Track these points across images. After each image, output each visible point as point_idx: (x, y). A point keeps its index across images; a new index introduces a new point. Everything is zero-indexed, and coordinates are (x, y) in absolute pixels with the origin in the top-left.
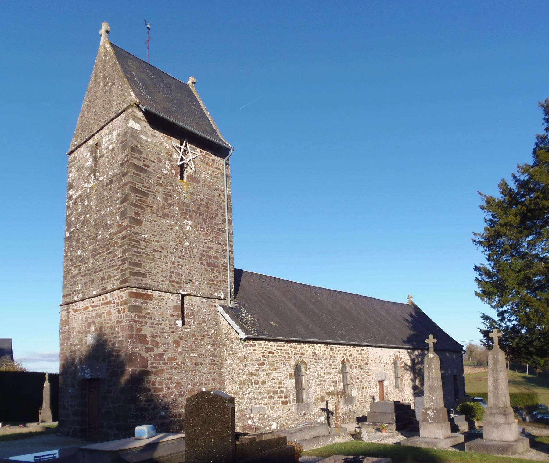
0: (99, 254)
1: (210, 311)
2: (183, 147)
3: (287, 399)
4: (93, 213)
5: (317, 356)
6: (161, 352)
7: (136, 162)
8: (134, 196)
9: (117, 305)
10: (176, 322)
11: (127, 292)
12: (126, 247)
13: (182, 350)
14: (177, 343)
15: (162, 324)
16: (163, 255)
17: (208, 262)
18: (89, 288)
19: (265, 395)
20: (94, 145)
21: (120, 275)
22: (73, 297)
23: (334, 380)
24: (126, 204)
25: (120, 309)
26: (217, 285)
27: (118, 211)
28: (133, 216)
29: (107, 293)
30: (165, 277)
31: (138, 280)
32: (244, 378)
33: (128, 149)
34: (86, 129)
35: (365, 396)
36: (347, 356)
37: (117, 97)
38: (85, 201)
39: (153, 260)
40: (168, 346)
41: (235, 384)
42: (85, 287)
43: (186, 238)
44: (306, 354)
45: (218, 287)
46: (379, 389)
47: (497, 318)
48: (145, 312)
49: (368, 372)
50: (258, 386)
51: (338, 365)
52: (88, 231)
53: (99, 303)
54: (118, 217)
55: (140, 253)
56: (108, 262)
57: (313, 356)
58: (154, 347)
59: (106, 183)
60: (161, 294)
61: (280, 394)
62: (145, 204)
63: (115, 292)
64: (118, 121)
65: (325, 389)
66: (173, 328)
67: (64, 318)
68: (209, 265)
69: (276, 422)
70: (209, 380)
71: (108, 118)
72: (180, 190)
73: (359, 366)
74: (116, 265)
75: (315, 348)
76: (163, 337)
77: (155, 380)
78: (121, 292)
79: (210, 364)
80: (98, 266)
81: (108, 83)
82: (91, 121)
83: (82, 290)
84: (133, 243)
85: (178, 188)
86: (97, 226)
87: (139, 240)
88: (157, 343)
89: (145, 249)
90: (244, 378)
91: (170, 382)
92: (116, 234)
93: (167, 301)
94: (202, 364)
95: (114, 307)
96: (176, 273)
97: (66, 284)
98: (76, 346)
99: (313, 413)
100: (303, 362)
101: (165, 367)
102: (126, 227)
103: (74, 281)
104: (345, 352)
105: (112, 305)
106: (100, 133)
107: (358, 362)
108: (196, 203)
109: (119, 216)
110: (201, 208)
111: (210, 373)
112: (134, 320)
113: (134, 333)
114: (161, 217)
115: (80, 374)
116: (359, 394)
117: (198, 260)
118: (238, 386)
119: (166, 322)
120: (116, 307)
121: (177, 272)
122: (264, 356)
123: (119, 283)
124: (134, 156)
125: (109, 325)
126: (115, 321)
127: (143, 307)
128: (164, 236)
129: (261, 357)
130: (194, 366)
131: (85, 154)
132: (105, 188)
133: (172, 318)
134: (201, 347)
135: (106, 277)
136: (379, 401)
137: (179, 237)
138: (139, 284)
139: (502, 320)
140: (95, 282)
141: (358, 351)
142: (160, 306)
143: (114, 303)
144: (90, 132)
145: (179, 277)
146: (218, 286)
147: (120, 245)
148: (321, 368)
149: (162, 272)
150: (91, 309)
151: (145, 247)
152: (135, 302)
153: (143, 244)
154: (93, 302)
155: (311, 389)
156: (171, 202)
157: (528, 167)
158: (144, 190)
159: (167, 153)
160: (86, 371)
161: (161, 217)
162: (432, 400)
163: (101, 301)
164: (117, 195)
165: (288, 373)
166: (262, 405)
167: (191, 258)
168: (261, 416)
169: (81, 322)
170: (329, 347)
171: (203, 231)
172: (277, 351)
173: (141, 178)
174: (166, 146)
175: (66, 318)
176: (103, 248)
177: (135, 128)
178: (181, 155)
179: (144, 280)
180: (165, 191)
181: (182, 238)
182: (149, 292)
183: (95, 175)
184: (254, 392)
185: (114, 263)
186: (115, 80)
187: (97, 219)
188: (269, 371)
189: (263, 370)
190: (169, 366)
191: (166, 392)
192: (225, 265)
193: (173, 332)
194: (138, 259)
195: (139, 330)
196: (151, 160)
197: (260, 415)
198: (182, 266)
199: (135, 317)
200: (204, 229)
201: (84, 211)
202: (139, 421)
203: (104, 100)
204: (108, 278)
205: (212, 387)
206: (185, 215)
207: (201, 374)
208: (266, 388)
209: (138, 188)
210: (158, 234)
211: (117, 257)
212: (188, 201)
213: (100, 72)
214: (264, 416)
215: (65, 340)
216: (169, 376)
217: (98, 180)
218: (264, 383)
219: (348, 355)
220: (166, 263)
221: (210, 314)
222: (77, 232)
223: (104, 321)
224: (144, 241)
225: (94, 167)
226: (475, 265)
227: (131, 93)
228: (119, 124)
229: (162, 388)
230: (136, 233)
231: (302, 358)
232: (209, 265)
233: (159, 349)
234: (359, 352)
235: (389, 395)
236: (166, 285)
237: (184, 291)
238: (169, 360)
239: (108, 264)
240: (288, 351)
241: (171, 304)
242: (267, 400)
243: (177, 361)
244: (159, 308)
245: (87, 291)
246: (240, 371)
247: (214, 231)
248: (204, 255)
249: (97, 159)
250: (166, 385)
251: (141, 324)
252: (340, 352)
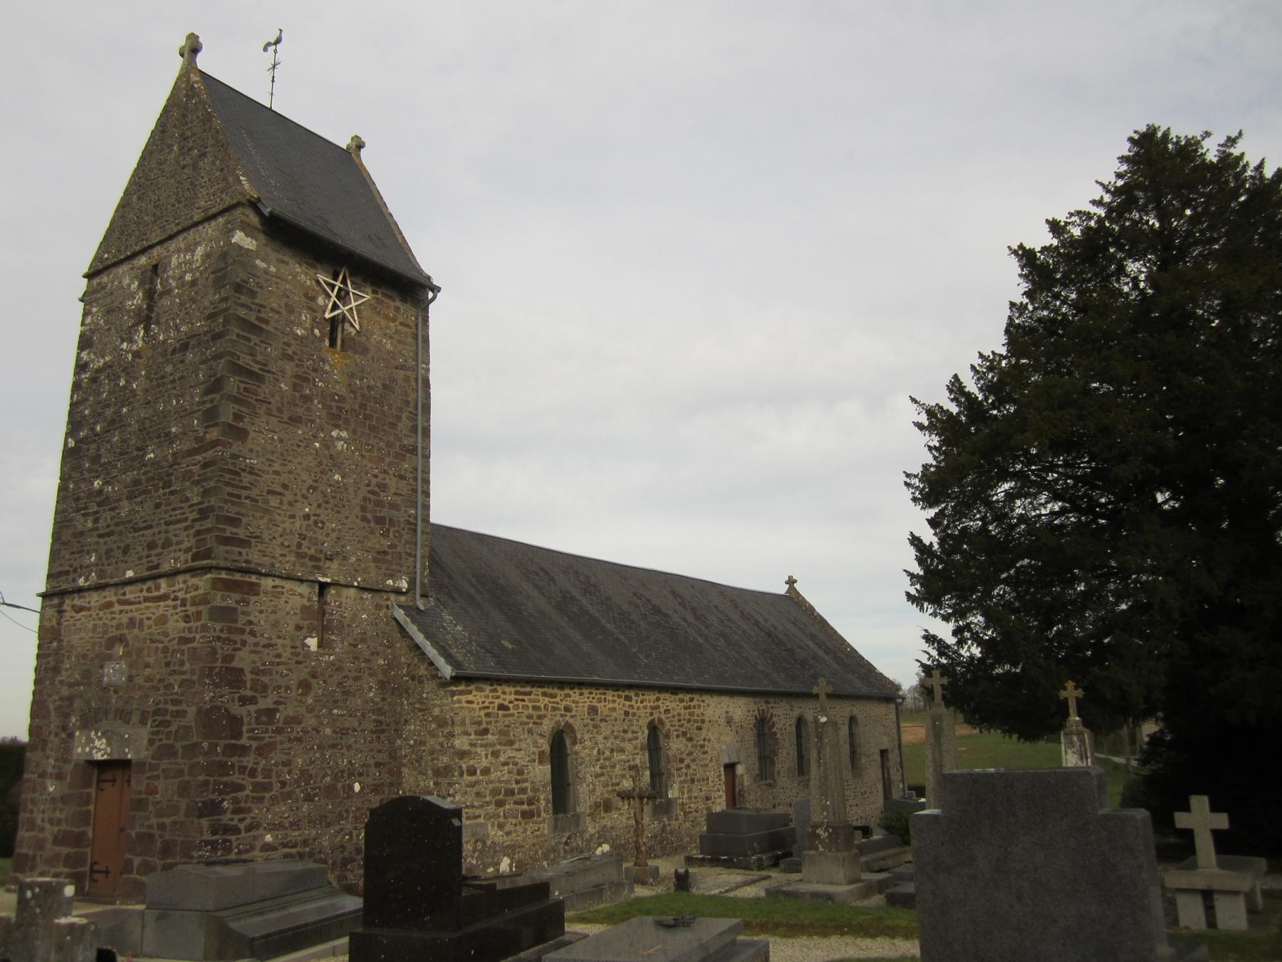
0: (145, 492)
1: (376, 618)
2: (338, 284)
3: (534, 807)
4: (136, 405)
5: (597, 714)
6: (272, 706)
7: (242, 312)
8: (234, 382)
9: (183, 604)
10: (306, 641)
11: (208, 579)
12: (212, 484)
13: (316, 701)
14: (305, 686)
15: (276, 645)
16: (285, 500)
17: (378, 515)
18: (116, 563)
19: (488, 799)
20: (151, 267)
21: (193, 541)
22: (74, 580)
23: (632, 763)
24: (217, 396)
25: (189, 613)
26: (394, 562)
27: (196, 408)
28: (230, 421)
30: (289, 546)
31: (233, 553)
32: (445, 761)
33: (228, 287)
34: (133, 231)
35: (695, 798)
36: (660, 713)
37: (210, 180)
38: (118, 378)
39: (266, 511)
40: (286, 692)
41: (426, 774)
42: (107, 559)
43: (336, 466)
44: (575, 709)
45: (397, 567)
46: (726, 783)
47: (951, 640)
48: (242, 619)
49: (702, 746)
50: (473, 779)
51: (640, 733)
52: (124, 441)
53: (139, 597)
54: (196, 421)
55: (239, 497)
56: (166, 512)
57: (589, 714)
58: (258, 696)
59: (172, 348)
60: (278, 582)
61: (518, 797)
62: (255, 397)
63: (180, 578)
64: (210, 229)
65: (613, 784)
66: (299, 654)
67: (47, 624)
68: (380, 521)
69: (508, 856)
70: (369, 766)
71: (186, 219)
72: (327, 368)
73: (684, 734)
74: (186, 519)
75: (593, 695)
76: (277, 673)
77: (255, 766)
79: (372, 731)
80: (142, 517)
81: (190, 150)
82: (146, 218)
83: (97, 565)
84: (228, 476)
85: (324, 364)
86: (144, 433)
87: (239, 471)
88: (265, 687)
89: (250, 489)
90: (445, 761)
91: (286, 769)
92: (190, 456)
93: (290, 597)
94: (355, 730)
95: (175, 607)
96: (310, 538)
97: (60, 550)
98: (74, 686)
99: (587, 836)
100: (568, 725)
101: (279, 738)
102: (214, 444)
103: (79, 545)
104: (656, 704)
105: (170, 602)
106: (166, 245)
107: (682, 726)
108: (358, 395)
109: (198, 419)
110: (369, 404)
111: (371, 750)
112: (219, 638)
113: (218, 664)
114: (286, 423)
115: (79, 750)
116: (683, 793)
117: (357, 511)
118: (431, 778)
119: (285, 642)
120: (180, 609)
121: (314, 535)
122: (488, 715)
123: (190, 557)
124: (239, 302)
125: (161, 646)
126: (174, 638)
127: (240, 609)
128: (289, 461)
129: (483, 716)
130: (339, 735)
131: (126, 281)
132: (169, 357)
133: (297, 633)
134: (354, 695)
135: (160, 543)
136: (725, 808)
137: (320, 463)
138: (234, 561)
139: (961, 642)
140: (130, 551)
141: (682, 701)
142: (273, 608)
143: (175, 599)
144: (143, 240)
145: (316, 547)
146: (396, 564)
147: (196, 478)
148: (605, 738)
149: (281, 536)
151: (251, 484)
152: (223, 599)
153: (246, 478)
154: (124, 594)
155: (584, 785)
156: (307, 392)
158: (256, 368)
159: (306, 295)
160: (97, 743)
161: (286, 423)
162: (825, 808)
164: (197, 376)
165: (536, 750)
166: (482, 820)
167: (344, 506)
168: (478, 843)
169: (90, 635)
170: (623, 694)
171: (368, 451)
172: (516, 703)
173: (252, 344)
174: (305, 282)
175: (54, 623)
176: (157, 482)
177: (246, 247)
178: (334, 298)
179: (244, 554)
180: (298, 370)
181: (327, 465)
182: (254, 579)
183: (147, 329)
184: (466, 792)
185: (180, 514)
186: (207, 147)
187: (147, 418)
188: (498, 747)
189: (485, 746)
190: (285, 734)
191: (277, 791)
192: (412, 520)
193: (298, 662)
194: (235, 509)
195: (229, 658)
196: (273, 310)
197: (476, 842)
198: (323, 523)
199: (221, 631)
200: (373, 447)
201: (116, 399)
202: (219, 854)
203: (179, 182)
204: (163, 544)
205: (374, 780)
206: (336, 419)
207: (352, 753)
208: (492, 782)
209: (243, 365)
210: (278, 458)
211: (189, 504)
212: (343, 391)
213: (175, 126)
214: (484, 843)
215: (46, 672)
216: (284, 758)
217: (155, 340)
218: (486, 771)
219: (662, 710)
220: (293, 516)
221: (376, 625)
222: (95, 441)
223: (149, 637)
224: (250, 473)
225: (146, 312)
226: (911, 533)
227: (242, 178)
228: (210, 235)
229: (270, 783)
230: (235, 457)
231: (567, 718)
232: (380, 521)
233: (267, 700)
234: (685, 704)
235: (746, 794)
236: (288, 564)
237: (324, 575)
238: (287, 724)
239: (164, 516)
240: (538, 704)
241: (297, 602)
242: (491, 808)
243: (302, 725)
244: (273, 612)
245: (110, 569)
246: (438, 747)
247: (392, 451)
248: (370, 500)
249: (156, 296)
250: (278, 777)
251: (233, 647)
252: (645, 703)
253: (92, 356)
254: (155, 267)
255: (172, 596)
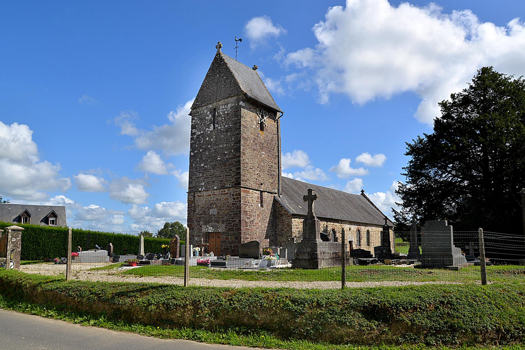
29: (226, 188)
70: (271, 235)
78: (235, 189)
81: (223, 76)
95: (230, 196)
122: (298, 224)
143: (230, 194)
150: (212, 196)
157: (511, 28)
163: (221, 193)
164: (232, 139)
169: (204, 202)
220: (255, 174)
232: (271, 175)
236: (254, 186)
253: (196, 131)
254: (215, 109)
255: (229, 193)
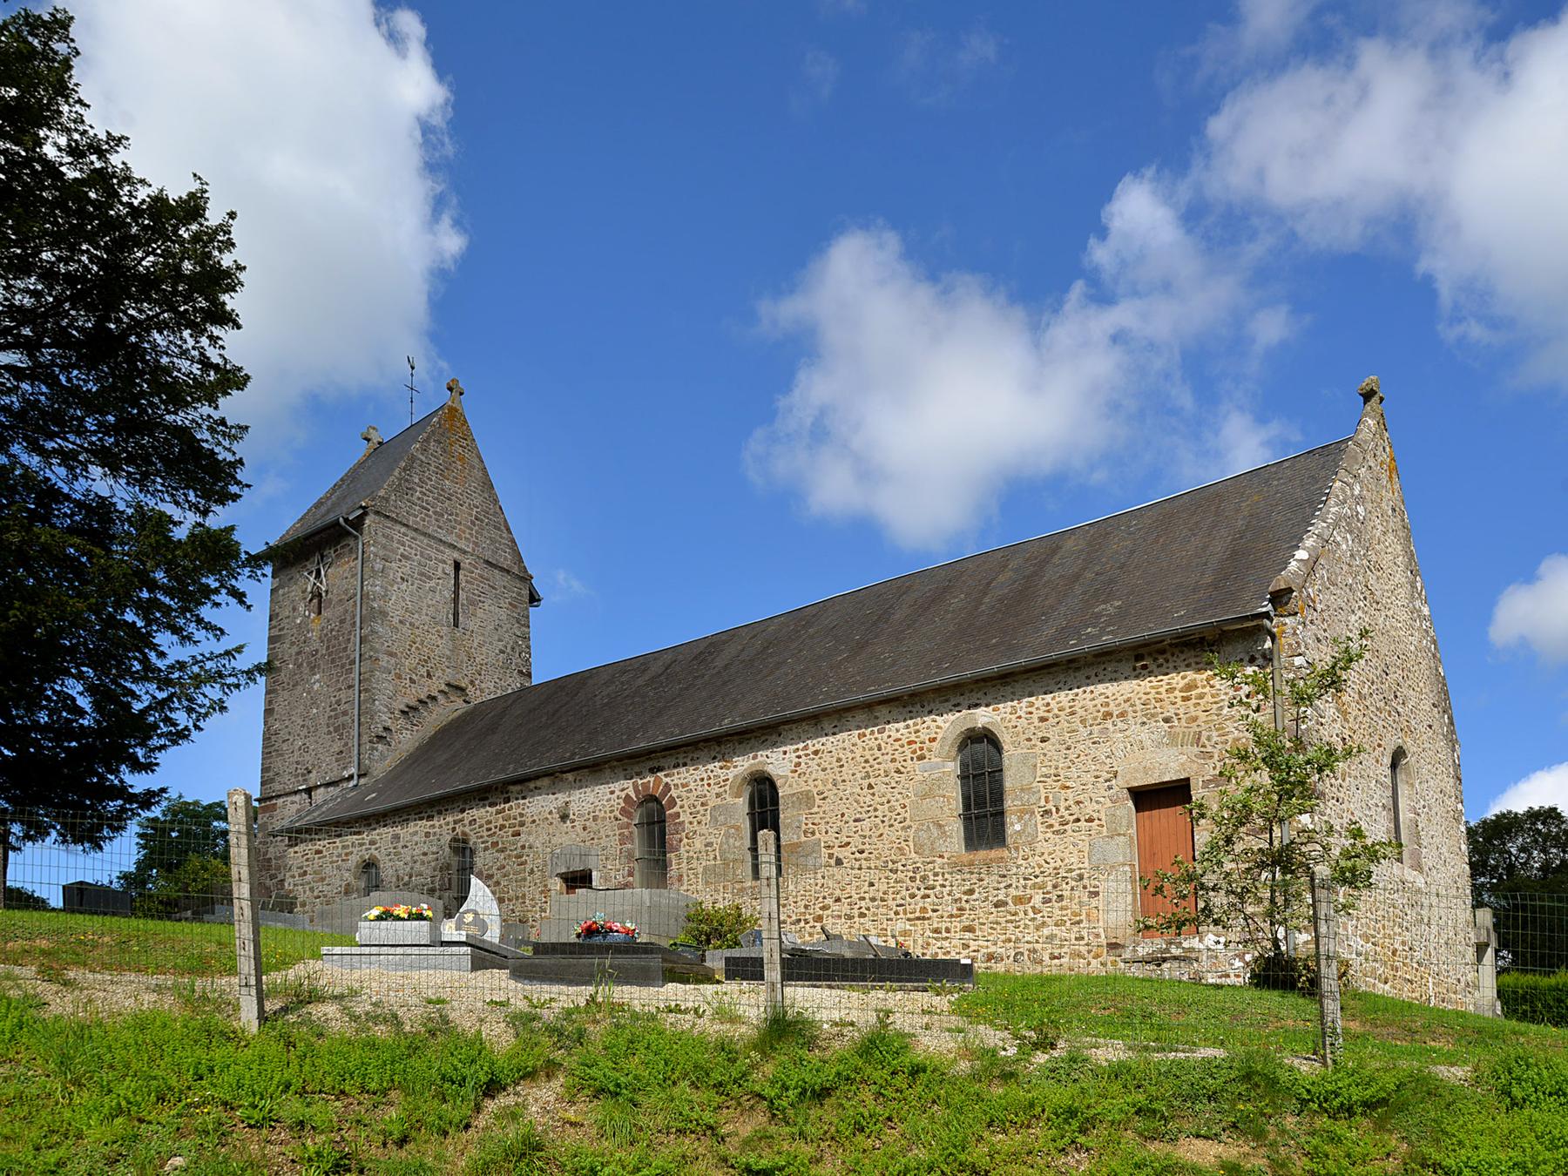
73: (495, 844)
